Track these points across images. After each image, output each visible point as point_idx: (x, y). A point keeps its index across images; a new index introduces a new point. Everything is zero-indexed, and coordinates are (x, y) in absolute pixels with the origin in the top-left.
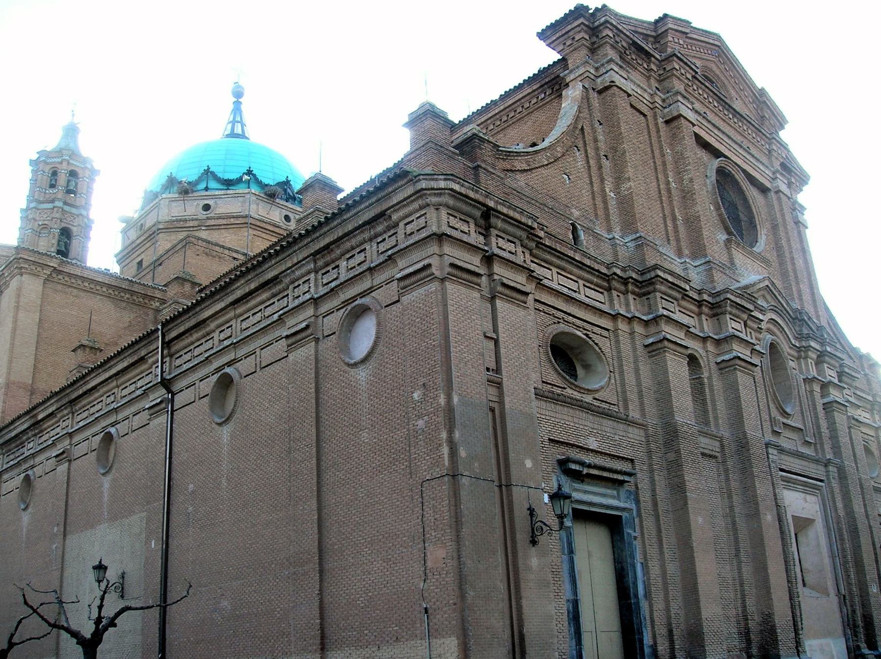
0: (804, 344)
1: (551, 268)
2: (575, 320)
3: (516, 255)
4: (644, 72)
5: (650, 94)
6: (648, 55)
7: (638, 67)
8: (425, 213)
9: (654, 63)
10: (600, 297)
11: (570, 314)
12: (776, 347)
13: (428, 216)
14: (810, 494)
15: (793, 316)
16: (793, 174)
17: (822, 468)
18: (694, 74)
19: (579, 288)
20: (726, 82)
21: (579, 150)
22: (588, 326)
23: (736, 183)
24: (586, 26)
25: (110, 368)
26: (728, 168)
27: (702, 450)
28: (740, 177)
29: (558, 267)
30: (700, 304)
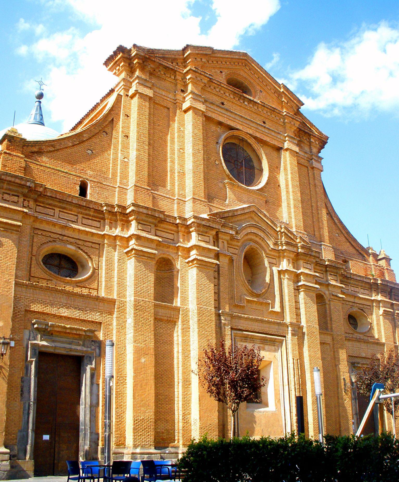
1: (54, 208)
2: (68, 239)
11: (64, 236)
18: (209, 79)
19: (77, 220)
20: (252, 81)
21: (107, 134)
22: (80, 243)
28: (251, 141)
29: (60, 207)
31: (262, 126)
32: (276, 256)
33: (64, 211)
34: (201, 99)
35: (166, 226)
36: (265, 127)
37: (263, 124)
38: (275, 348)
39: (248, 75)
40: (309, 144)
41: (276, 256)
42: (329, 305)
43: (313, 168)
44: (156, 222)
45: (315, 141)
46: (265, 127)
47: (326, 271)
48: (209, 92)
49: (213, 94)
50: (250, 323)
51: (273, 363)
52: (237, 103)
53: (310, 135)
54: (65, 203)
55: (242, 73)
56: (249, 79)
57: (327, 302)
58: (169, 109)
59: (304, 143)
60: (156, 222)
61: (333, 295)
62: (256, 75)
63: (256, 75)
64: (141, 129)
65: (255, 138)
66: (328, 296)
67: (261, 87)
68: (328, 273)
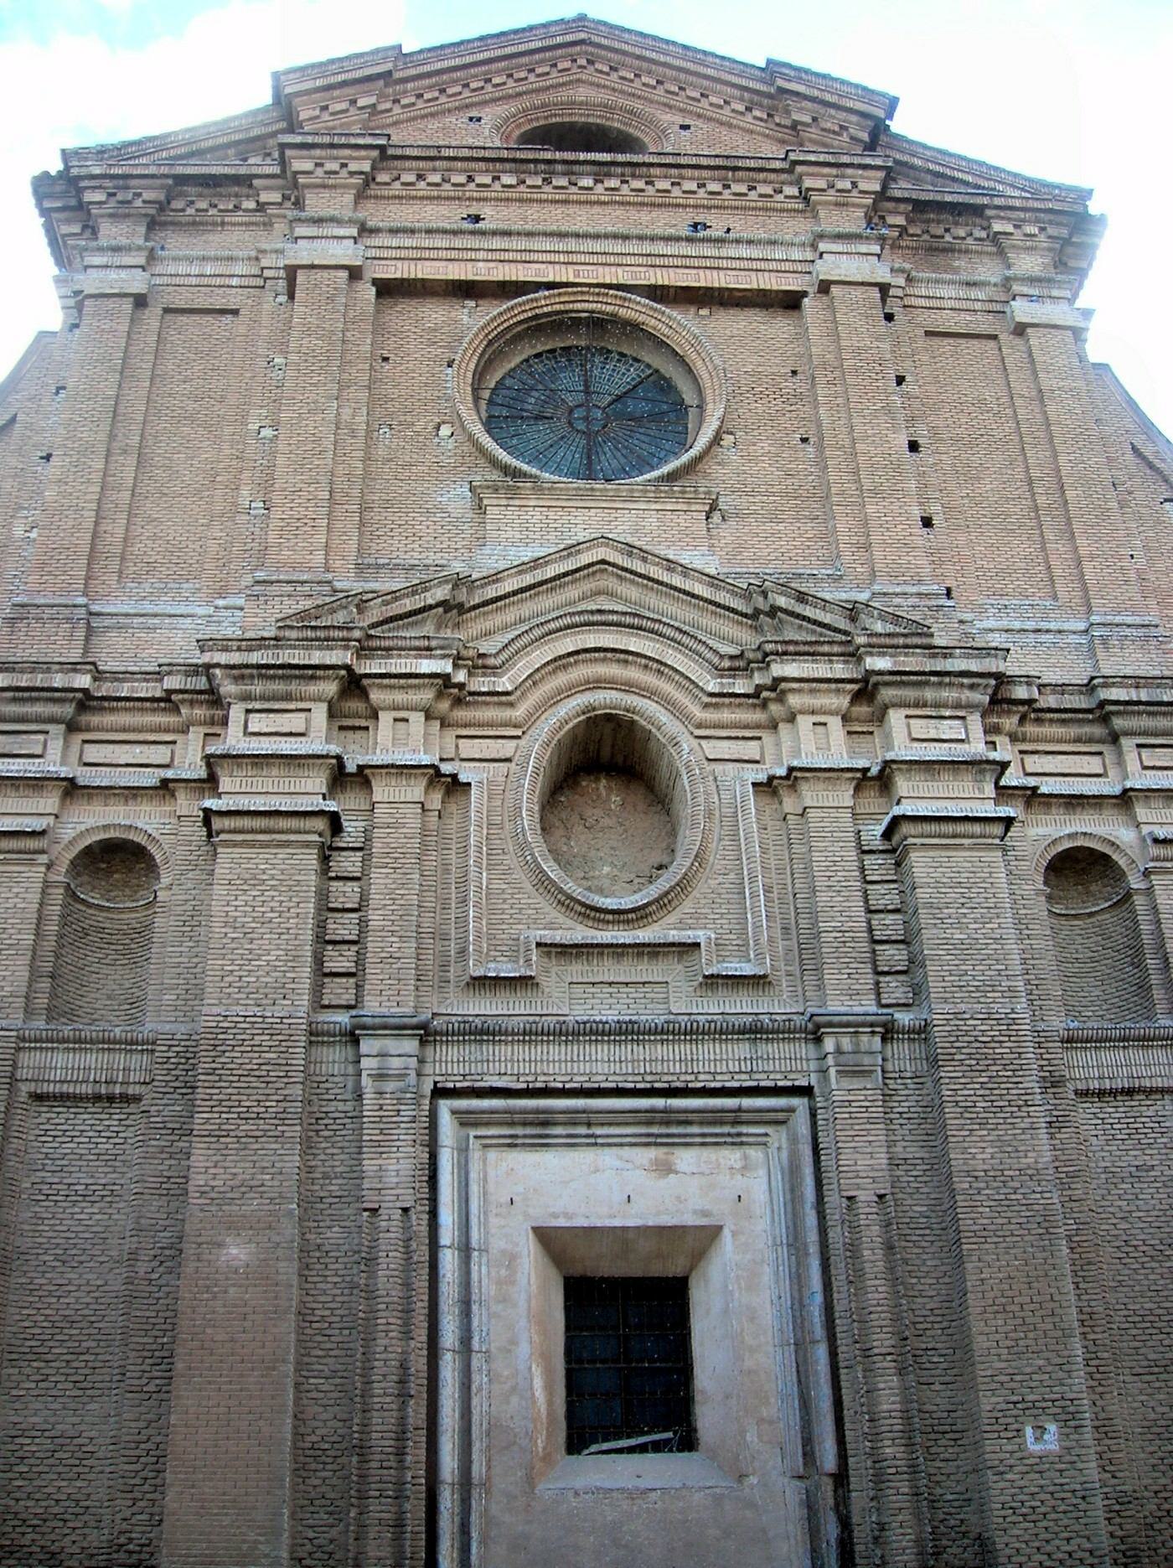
0: (758, 679)
3: (969, 742)
4: (253, 219)
5: (249, 259)
6: (245, 181)
7: (226, 219)
8: (174, 742)
9: (266, 188)
10: (1093, 765)
12: (633, 722)
13: (178, 748)
14: (609, 1145)
15: (750, 611)
16: (989, 212)
17: (805, 1050)
20: (638, 105)
23: (633, 329)
24: (58, 210)
25: (537, 1111)
26: (578, 306)
27: (32, 1087)
28: (638, 310)
30: (168, 701)
31: (473, 233)
32: (758, 726)
33: (292, 706)
34: (342, 232)
35: (109, 719)
36: (483, 233)
37: (471, 226)
38: (746, 1157)
39: (614, 90)
40: (994, 249)
41: (758, 726)
42: (1149, 891)
43: (1020, 330)
44: (68, 710)
45: (1016, 226)
46: (483, 233)
47: (1114, 738)
48: (400, 198)
49: (422, 198)
50: (556, 1051)
51: (734, 1234)
52: (544, 196)
53: (977, 211)
54: (570, 664)
55: (582, 93)
56: (622, 101)
57: (1135, 882)
58: (995, 337)
59: (967, 251)
60: (68, 710)
61: (1156, 841)
62: (645, 79)
63: (645, 79)
64: (962, 411)
65: (658, 293)
66: (1135, 853)
67: (681, 110)
68: (1127, 743)
